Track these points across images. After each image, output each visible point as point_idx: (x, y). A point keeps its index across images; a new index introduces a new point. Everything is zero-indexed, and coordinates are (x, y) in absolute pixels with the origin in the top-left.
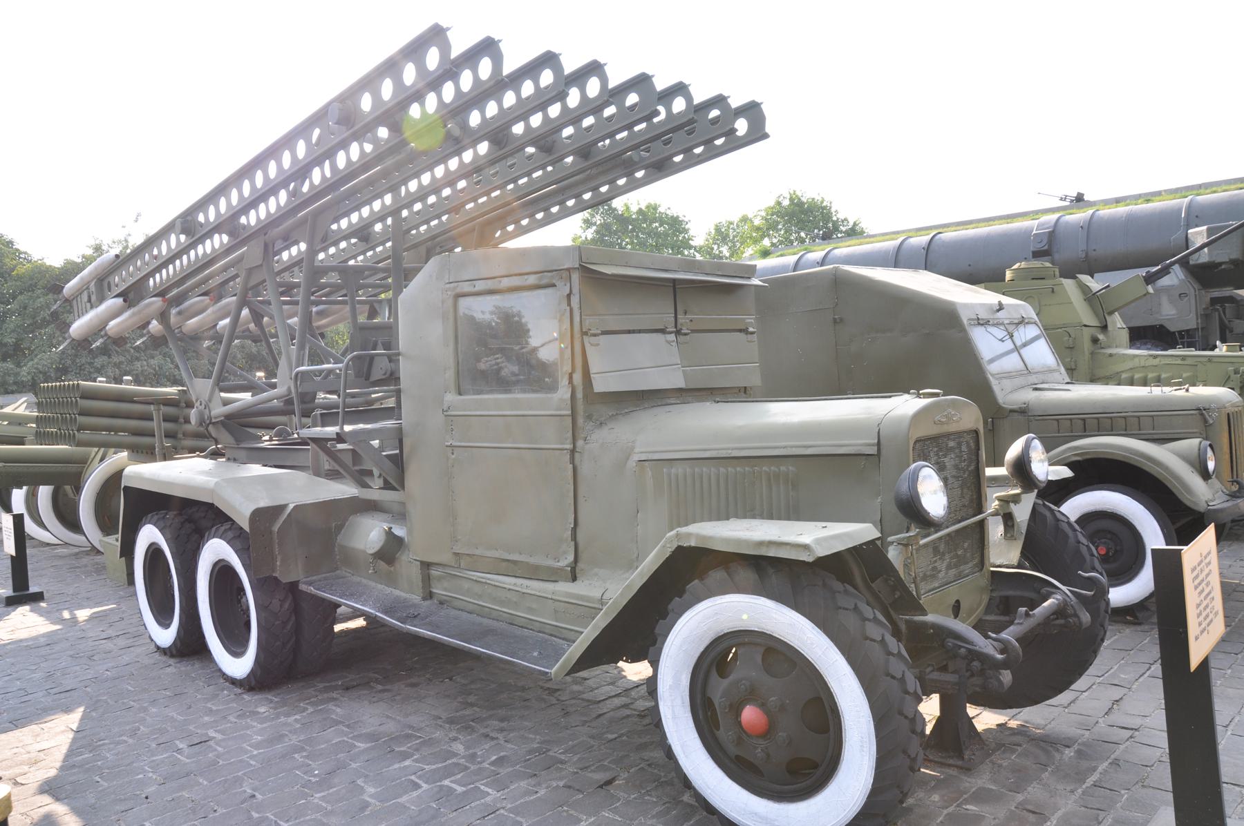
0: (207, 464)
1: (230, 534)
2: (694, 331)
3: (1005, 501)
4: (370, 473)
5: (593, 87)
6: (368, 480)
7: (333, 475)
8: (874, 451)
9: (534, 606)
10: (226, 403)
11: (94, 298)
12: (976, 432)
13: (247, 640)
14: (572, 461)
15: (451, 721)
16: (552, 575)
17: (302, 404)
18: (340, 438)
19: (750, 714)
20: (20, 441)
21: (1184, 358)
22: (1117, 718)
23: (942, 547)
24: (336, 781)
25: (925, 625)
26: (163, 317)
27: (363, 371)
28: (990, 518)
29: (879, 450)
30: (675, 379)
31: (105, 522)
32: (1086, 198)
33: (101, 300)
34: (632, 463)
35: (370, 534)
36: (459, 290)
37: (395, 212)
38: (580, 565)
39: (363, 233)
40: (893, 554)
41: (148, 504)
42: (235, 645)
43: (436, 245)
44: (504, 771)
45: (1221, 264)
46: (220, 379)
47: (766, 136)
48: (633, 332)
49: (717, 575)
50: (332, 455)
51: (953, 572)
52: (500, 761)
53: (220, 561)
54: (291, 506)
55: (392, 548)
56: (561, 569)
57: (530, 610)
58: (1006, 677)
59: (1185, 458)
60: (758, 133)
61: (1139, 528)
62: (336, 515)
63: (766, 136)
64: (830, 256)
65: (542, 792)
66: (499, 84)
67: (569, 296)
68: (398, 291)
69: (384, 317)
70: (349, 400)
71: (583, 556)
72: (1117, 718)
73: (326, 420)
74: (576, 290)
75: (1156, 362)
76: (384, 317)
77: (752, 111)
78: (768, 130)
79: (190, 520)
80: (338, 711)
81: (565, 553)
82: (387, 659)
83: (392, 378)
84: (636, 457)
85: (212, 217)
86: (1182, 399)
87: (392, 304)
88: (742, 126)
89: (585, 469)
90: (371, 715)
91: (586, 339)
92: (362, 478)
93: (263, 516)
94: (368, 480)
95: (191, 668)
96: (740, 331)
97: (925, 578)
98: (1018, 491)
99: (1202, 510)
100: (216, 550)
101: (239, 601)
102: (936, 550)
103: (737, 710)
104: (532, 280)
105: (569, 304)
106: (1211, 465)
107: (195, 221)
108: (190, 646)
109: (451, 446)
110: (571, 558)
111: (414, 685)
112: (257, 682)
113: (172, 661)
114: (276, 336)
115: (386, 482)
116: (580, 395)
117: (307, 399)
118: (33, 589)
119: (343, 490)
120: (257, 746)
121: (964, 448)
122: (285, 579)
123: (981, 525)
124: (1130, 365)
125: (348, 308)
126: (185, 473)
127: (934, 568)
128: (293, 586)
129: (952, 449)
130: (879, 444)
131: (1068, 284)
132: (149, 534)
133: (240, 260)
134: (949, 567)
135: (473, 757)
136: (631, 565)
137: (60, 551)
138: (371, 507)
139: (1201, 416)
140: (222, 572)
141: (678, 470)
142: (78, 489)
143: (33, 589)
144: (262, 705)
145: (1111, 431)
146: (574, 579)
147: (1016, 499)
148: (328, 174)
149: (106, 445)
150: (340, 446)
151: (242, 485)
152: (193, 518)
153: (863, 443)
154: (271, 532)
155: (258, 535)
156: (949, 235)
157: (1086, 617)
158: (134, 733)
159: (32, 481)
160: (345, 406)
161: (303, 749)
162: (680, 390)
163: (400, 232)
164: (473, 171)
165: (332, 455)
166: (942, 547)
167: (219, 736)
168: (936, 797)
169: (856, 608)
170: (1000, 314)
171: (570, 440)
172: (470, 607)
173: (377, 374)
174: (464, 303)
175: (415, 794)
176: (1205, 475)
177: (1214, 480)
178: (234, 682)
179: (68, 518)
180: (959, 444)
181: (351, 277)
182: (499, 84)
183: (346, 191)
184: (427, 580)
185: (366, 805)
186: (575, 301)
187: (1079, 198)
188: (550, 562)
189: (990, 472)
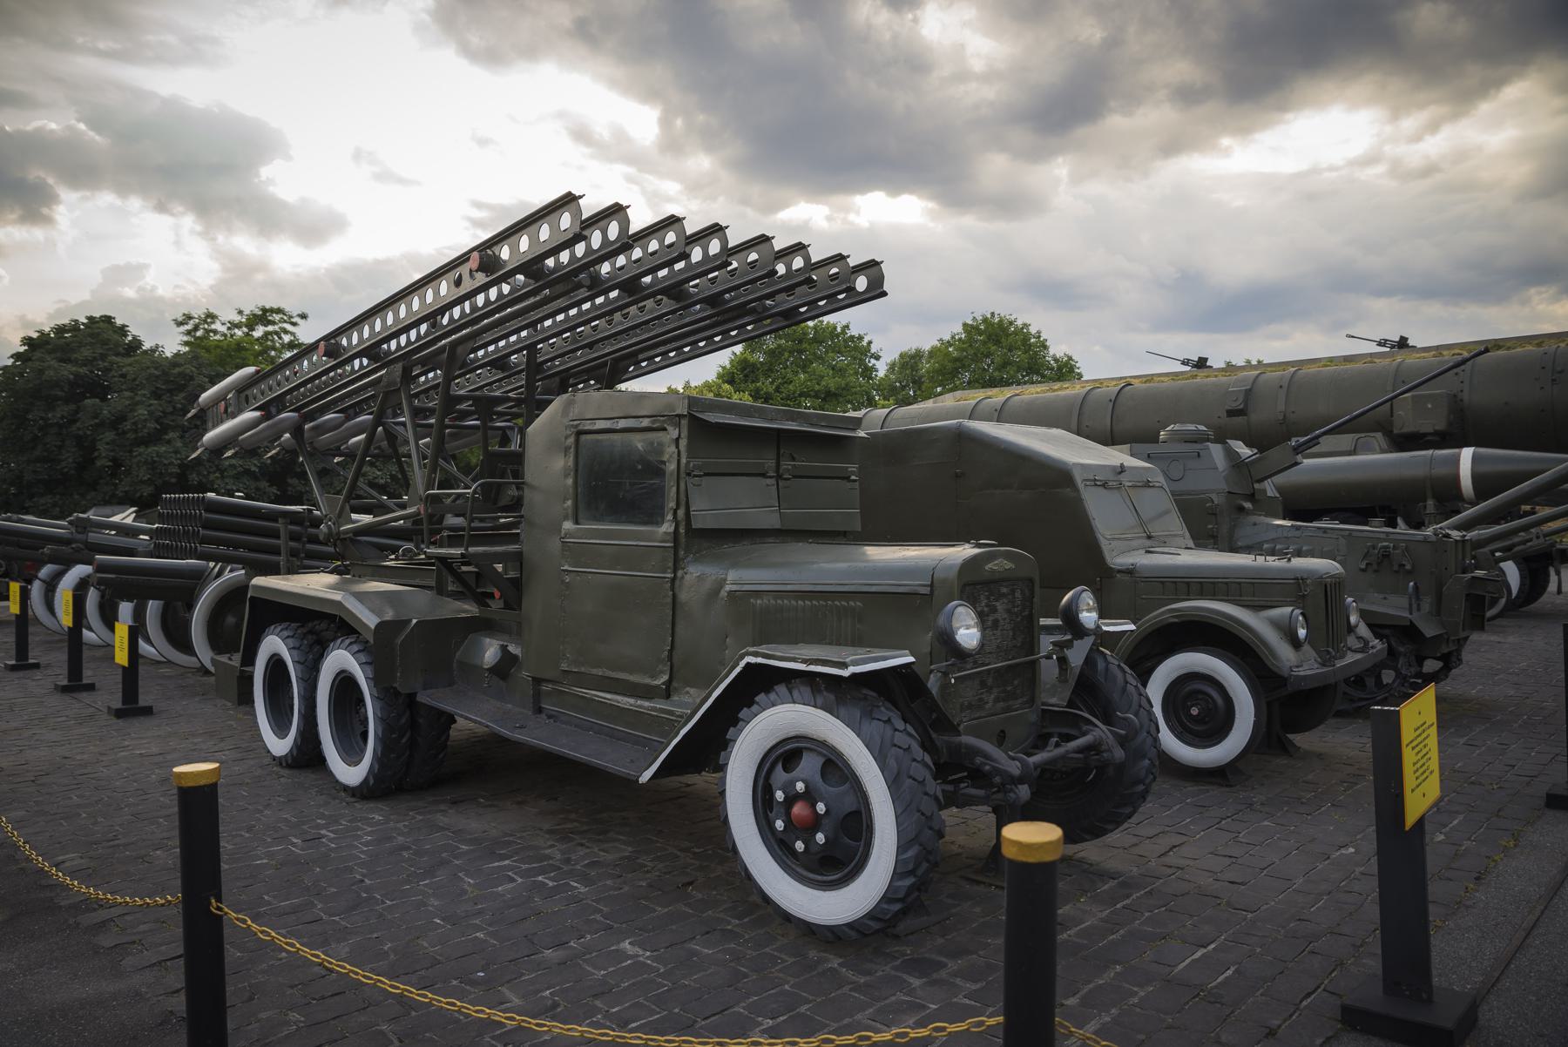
0: (332, 579)
1: (355, 648)
3: (1060, 646)
4: (491, 596)
5: (715, 247)
6: (489, 602)
7: (457, 596)
8: (926, 591)
12: (1031, 580)
13: (363, 751)
14: (673, 588)
15: (550, 832)
16: (647, 692)
18: (466, 559)
20: (131, 552)
21: (1325, 530)
22: (1171, 859)
23: (990, 681)
25: (960, 744)
26: (297, 431)
27: (491, 498)
28: (1043, 661)
30: (771, 520)
31: (218, 640)
32: (1410, 342)
33: (240, 411)
34: (723, 594)
37: (531, 348)
38: (675, 684)
39: (500, 363)
40: (933, 683)
42: (351, 754)
43: (564, 382)
45: (1425, 435)
47: (884, 294)
49: (781, 689)
50: (459, 577)
51: (1001, 704)
52: (592, 864)
53: (343, 671)
55: (506, 664)
56: (657, 687)
58: (1024, 792)
59: (1276, 624)
60: (877, 291)
61: (1197, 669)
63: (884, 294)
64: (981, 406)
65: (626, 888)
66: (625, 244)
68: (529, 422)
69: (514, 446)
70: (476, 524)
72: (1171, 859)
73: (454, 541)
74: (685, 433)
75: (1298, 533)
76: (514, 446)
77: (871, 266)
78: (885, 288)
79: (311, 632)
80: (442, 819)
82: (496, 771)
83: (516, 505)
85: (355, 340)
86: (1280, 570)
87: (522, 431)
88: (861, 283)
90: (474, 822)
91: (690, 480)
92: (482, 599)
94: (489, 602)
95: (307, 777)
97: (970, 706)
98: (1069, 637)
99: (1285, 673)
100: (340, 659)
102: (983, 684)
104: (646, 423)
106: (1302, 633)
107: (339, 345)
108: (308, 756)
111: (519, 803)
113: (286, 772)
114: (409, 456)
115: (506, 603)
116: (682, 531)
117: (436, 520)
118: (144, 701)
119: (469, 609)
120: (367, 844)
121: (1018, 594)
122: (404, 690)
123: (1033, 665)
124: (1273, 535)
125: (480, 434)
126: (316, 584)
127: (981, 700)
128: (411, 697)
129: (1004, 595)
130: (932, 585)
131: (1216, 450)
132: (274, 644)
133: (379, 379)
134: (997, 700)
135: (568, 861)
136: (710, 682)
137: (164, 670)
138: (484, 626)
139: (1296, 589)
142: (190, 607)
143: (144, 701)
144: (377, 813)
145: (1213, 596)
147: (1069, 644)
148: (468, 311)
149: (227, 560)
150: (464, 568)
151: (366, 599)
152: (318, 627)
153: (918, 584)
155: (381, 647)
156: (1305, 370)
157: (1119, 754)
158: (250, 829)
159: (139, 596)
161: (409, 848)
163: (534, 368)
164: (607, 313)
165: (459, 577)
166: (990, 681)
168: (978, 910)
169: (889, 721)
170: (1123, 478)
173: (503, 502)
174: (583, 438)
175: (511, 885)
176: (1296, 643)
177: (1306, 648)
178: (346, 788)
179: (179, 639)
180: (1013, 591)
181: (485, 406)
182: (625, 244)
183: (479, 327)
184: (537, 696)
185: (464, 892)
186: (683, 443)
187: (1403, 343)
189: (1044, 621)
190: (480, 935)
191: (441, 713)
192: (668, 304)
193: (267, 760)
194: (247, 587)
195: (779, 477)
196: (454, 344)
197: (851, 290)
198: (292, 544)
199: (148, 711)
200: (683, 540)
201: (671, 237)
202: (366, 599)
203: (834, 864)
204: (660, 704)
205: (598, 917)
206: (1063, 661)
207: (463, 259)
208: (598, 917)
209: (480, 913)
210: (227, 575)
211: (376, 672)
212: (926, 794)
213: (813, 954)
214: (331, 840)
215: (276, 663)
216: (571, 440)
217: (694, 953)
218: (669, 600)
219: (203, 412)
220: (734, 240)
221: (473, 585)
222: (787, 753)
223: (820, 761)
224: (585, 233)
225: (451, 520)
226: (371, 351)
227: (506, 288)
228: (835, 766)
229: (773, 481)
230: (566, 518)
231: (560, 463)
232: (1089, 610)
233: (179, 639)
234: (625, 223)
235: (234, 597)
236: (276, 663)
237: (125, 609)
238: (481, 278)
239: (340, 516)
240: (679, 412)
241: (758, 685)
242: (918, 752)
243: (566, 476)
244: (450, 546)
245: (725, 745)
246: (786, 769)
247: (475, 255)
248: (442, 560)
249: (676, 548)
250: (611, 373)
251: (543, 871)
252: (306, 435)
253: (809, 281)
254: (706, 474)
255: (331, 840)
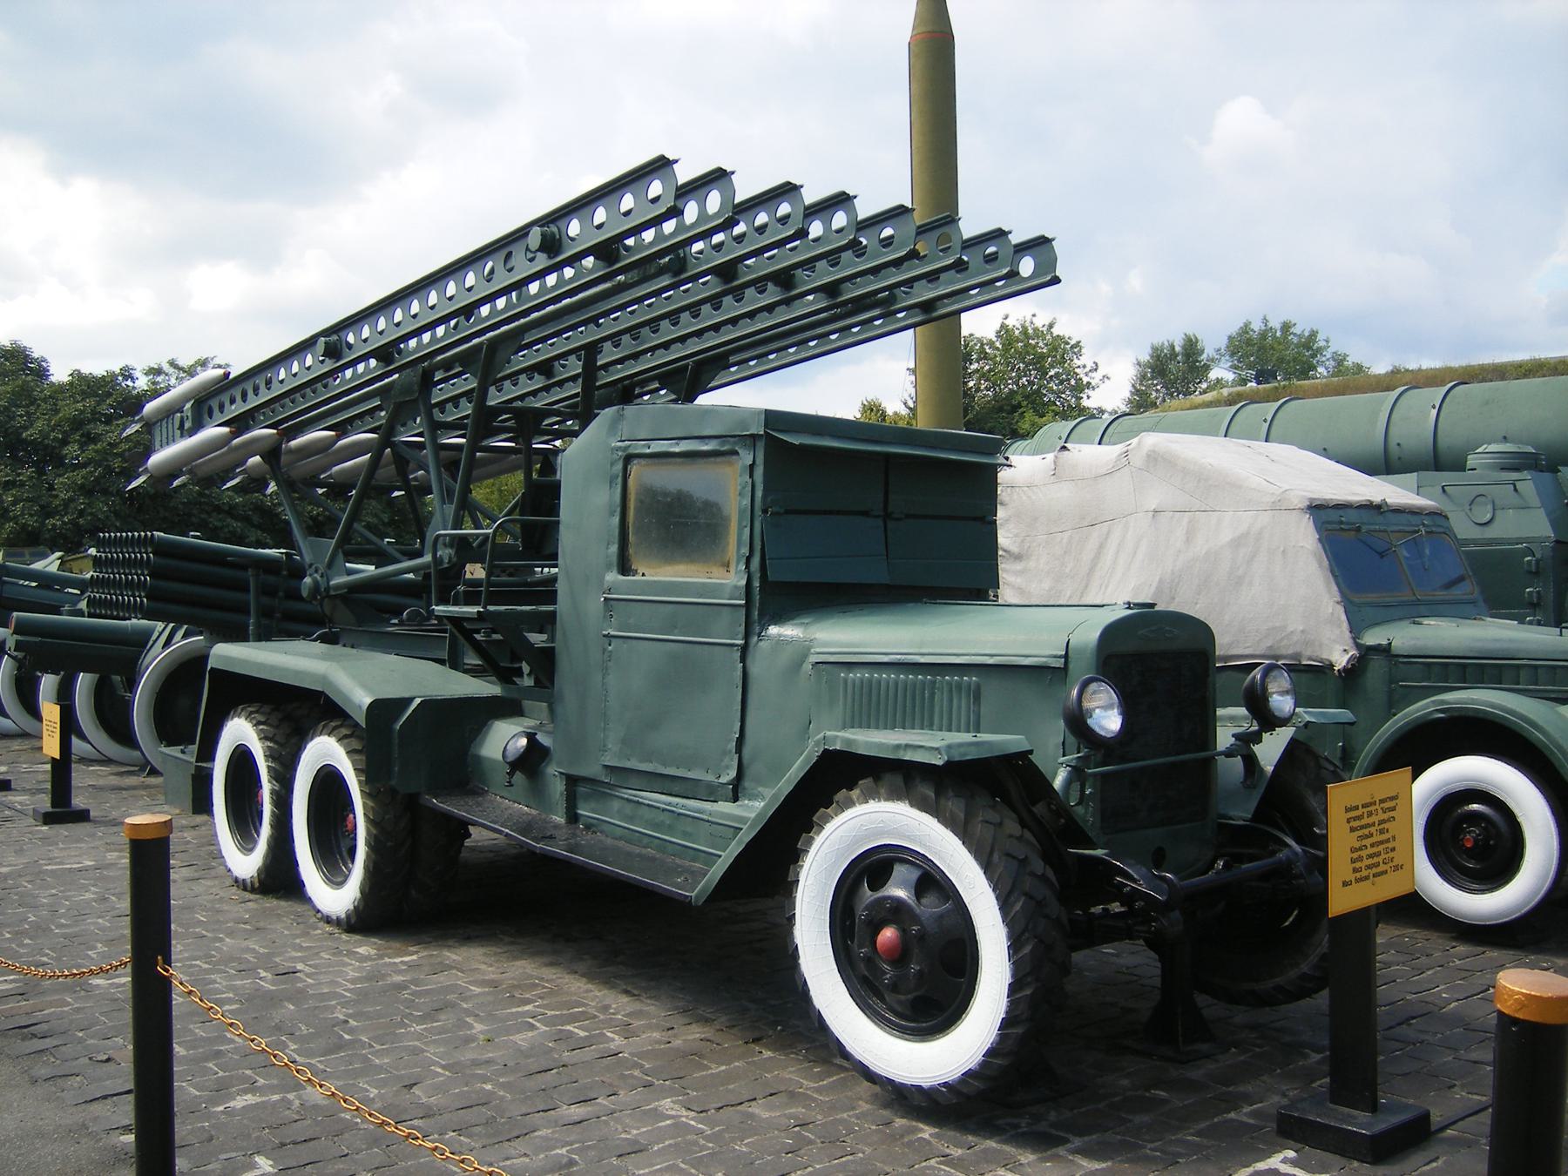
2: (908, 516)
5: (714, 201)
7: (474, 672)
8: (1060, 663)
9: (689, 829)
10: (350, 572)
11: (188, 425)
14: (743, 659)
17: (446, 581)
19: (888, 934)
24: (443, 1017)
29: (1066, 663)
33: (198, 426)
34: (807, 667)
35: (504, 739)
36: (631, 451)
41: (241, 691)
42: (335, 877)
43: (626, 393)
44: (637, 1023)
46: (346, 538)
48: (830, 512)
54: (418, 701)
55: (531, 760)
57: (686, 835)
61: (1516, 811)
62: (470, 717)
63: (1056, 281)
67: (752, 467)
71: (750, 772)
73: (470, 599)
77: (1040, 245)
81: (727, 767)
84: (813, 659)
88: (1027, 266)
89: (755, 669)
92: (506, 676)
93: (384, 709)
96: (975, 519)
100: (324, 750)
101: (345, 818)
103: (877, 928)
105: (751, 476)
108: (279, 879)
109: (607, 636)
110: (733, 774)
112: (361, 922)
116: (757, 584)
118: (78, 802)
120: (353, 981)
130: (1066, 656)
132: (239, 731)
140: (328, 780)
141: (856, 675)
142: (132, 684)
143: (78, 802)
146: (735, 800)
147: (1256, 738)
152: (296, 711)
154: (391, 730)
155: (378, 733)
160: (490, 584)
162: (888, 586)
167: (307, 969)
171: (741, 635)
172: (619, 831)
175: (530, 1034)
181: (527, 422)
186: (759, 472)
188: (710, 778)
190: (489, 1087)
191: (448, 818)
192: (773, 294)
193: (229, 882)
194: (205, 658)
195: (887, 516)
196: (493, 343)
197: (1013, 274)
198: (265, 600)
199: (82, 816)
200: (757, 598)
201: (784, 209)
202: (359, 677)
203: (929, 1004)
204: (725, 807)
205: (636, 1073)
206: (1251, 762)
207: (521, 234)
208: (636, 1073)
209: (488, 1062)
210: (179, 642)
211: (369, 762)
212: (1047, 916)
213: (900, 1122)
214: (308, 975)
215: (242, 757)
216: (620, 466)
217: (752, 1116)
218: (739, 673)
219: (149, 426)
220: (864, 210)
221: (496, 665)
222: (873, 866)
223: (915, 874)
224: (680, 204)
225: (476, 571)
226: (385, 353)
227: (569, 272)
228: (932, 881)
229: (880, 522)
230: (608, 568)
231: (604, 497)
232: (1282, 693)
233: (119, 729)
234: (729, 192)
235: (188, 671)
236: (242, 757)
237: (48, 683)
238: (542, 261)
239: (330, 565)
240: (753, 431)
241: (836, 777)
242: (1038, 866)
243: (612, 514)
244: (467, 604)
245: (794, 856)
246: (873, 888)
247: (536, 231)
248: (456, 621)
249: (748, 606)
250: (690, 379)
251: (573, 1019)
252: (284, 459)
253: (854, 245)
254: (787, 512)
255: (308, 975)
